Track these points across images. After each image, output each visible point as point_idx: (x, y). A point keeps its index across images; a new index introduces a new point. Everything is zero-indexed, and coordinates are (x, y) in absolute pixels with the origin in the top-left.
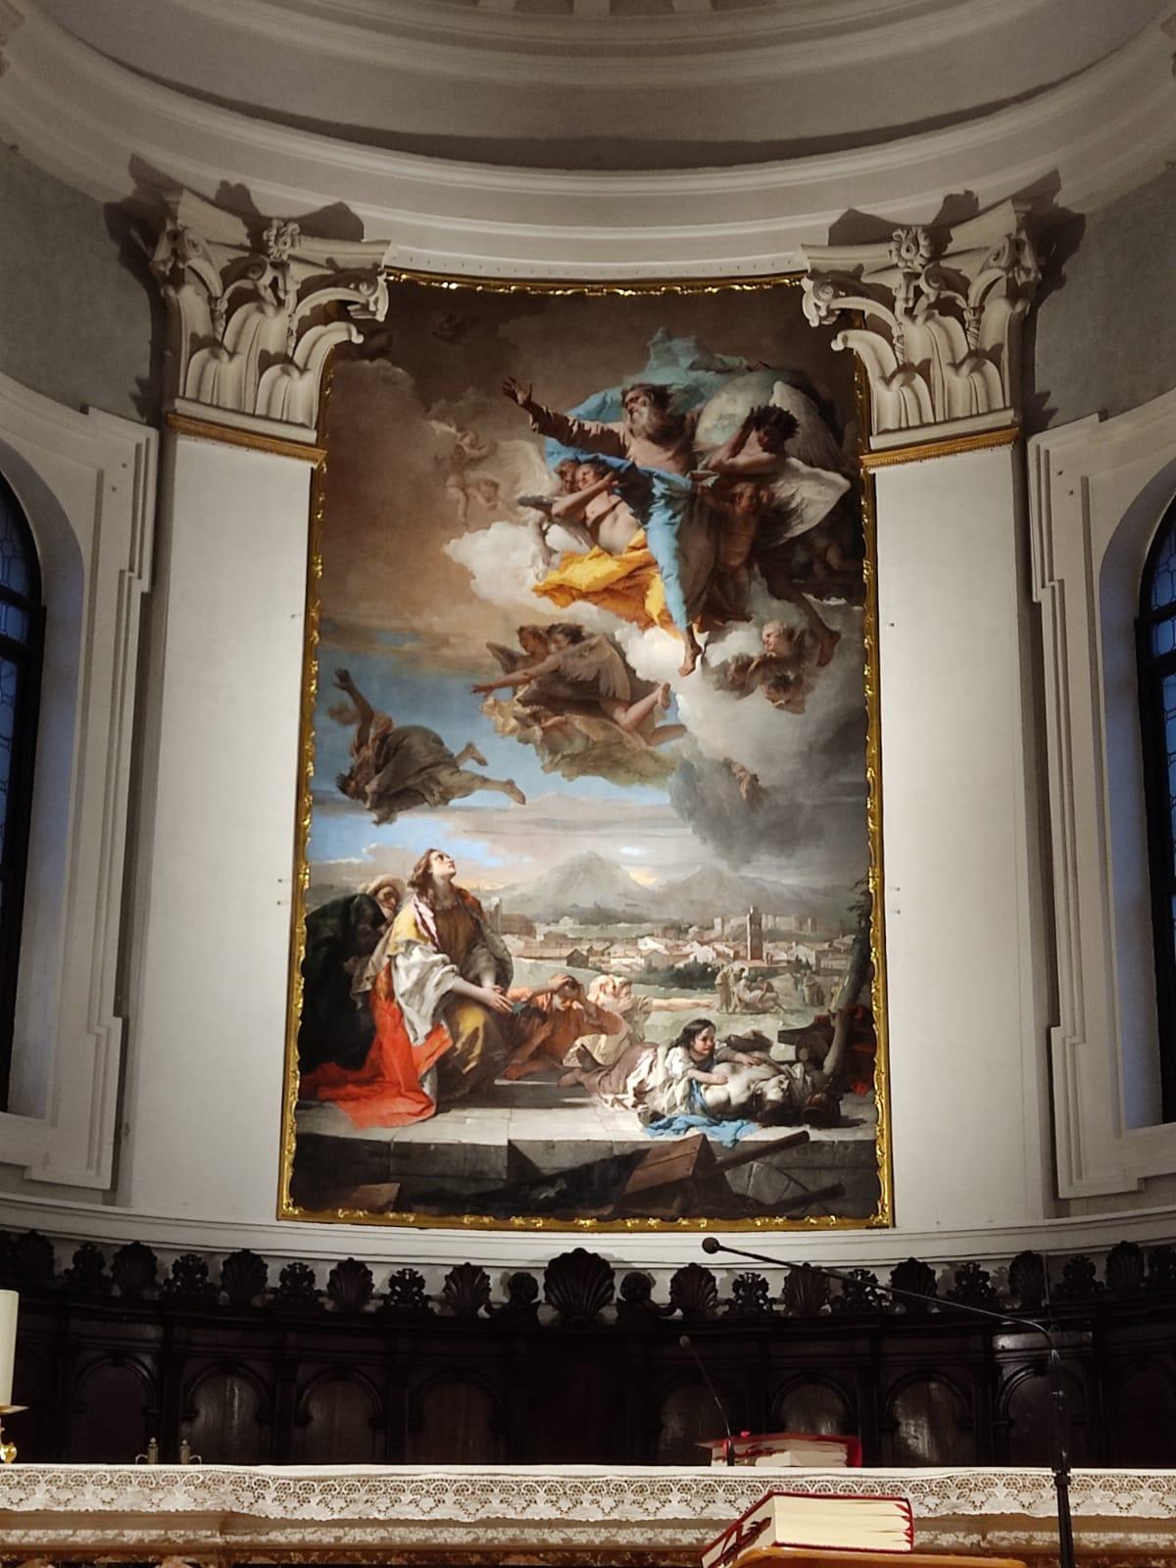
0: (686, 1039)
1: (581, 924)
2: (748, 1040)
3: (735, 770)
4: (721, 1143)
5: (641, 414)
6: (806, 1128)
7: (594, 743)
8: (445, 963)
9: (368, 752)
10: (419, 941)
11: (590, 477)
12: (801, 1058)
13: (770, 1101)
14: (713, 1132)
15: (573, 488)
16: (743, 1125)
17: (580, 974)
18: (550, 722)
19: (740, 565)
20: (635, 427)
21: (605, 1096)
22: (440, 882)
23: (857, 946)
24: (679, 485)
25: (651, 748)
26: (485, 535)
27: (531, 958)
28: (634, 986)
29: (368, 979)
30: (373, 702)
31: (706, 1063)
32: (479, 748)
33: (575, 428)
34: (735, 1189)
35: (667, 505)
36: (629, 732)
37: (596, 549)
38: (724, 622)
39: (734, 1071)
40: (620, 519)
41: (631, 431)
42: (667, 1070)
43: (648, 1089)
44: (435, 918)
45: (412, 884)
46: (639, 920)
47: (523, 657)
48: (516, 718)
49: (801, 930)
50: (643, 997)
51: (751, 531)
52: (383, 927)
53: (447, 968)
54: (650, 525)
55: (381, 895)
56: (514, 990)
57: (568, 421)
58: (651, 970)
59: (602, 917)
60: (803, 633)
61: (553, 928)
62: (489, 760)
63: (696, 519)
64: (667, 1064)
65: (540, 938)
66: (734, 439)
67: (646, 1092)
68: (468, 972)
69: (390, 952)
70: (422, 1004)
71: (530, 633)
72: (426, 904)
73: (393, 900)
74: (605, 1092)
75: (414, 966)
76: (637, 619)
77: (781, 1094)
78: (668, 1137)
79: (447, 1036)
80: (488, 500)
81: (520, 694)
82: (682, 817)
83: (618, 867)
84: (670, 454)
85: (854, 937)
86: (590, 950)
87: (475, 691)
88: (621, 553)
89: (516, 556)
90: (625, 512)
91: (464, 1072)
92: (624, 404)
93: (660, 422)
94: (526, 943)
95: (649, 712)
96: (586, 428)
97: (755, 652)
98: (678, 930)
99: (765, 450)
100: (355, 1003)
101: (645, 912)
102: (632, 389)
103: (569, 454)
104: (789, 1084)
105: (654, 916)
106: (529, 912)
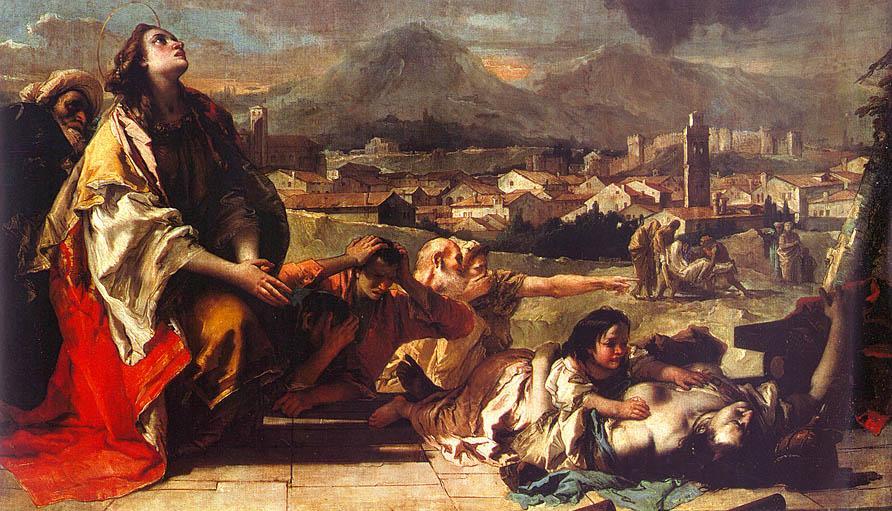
8: (173, 223)
14: (624, 499)
16: (675, 486)
21: (444, 441)
22: (161, 82)
27: (318, 210)
29: (44, 251)
31: (612, 383)
39: (661, 396)
42: (549, 396)
43: (517, 427)
44: (152, 146)
45: (113, 86)
46: (496, 142)
49: (775, 152)
53: (177, 231)
55: (61, 106)
58: (519, 225)
61: (354, 158)
65: (333, 175)
69: (80, 203)
72: (138, 121)
73: (81, 115)
74: (445, 434)
75: (121, 227)
77: (738, 434)
86: (417, 196)
94: (310, 184)
98: (562, 157)
101: (510, 128)
106: (315, 130)
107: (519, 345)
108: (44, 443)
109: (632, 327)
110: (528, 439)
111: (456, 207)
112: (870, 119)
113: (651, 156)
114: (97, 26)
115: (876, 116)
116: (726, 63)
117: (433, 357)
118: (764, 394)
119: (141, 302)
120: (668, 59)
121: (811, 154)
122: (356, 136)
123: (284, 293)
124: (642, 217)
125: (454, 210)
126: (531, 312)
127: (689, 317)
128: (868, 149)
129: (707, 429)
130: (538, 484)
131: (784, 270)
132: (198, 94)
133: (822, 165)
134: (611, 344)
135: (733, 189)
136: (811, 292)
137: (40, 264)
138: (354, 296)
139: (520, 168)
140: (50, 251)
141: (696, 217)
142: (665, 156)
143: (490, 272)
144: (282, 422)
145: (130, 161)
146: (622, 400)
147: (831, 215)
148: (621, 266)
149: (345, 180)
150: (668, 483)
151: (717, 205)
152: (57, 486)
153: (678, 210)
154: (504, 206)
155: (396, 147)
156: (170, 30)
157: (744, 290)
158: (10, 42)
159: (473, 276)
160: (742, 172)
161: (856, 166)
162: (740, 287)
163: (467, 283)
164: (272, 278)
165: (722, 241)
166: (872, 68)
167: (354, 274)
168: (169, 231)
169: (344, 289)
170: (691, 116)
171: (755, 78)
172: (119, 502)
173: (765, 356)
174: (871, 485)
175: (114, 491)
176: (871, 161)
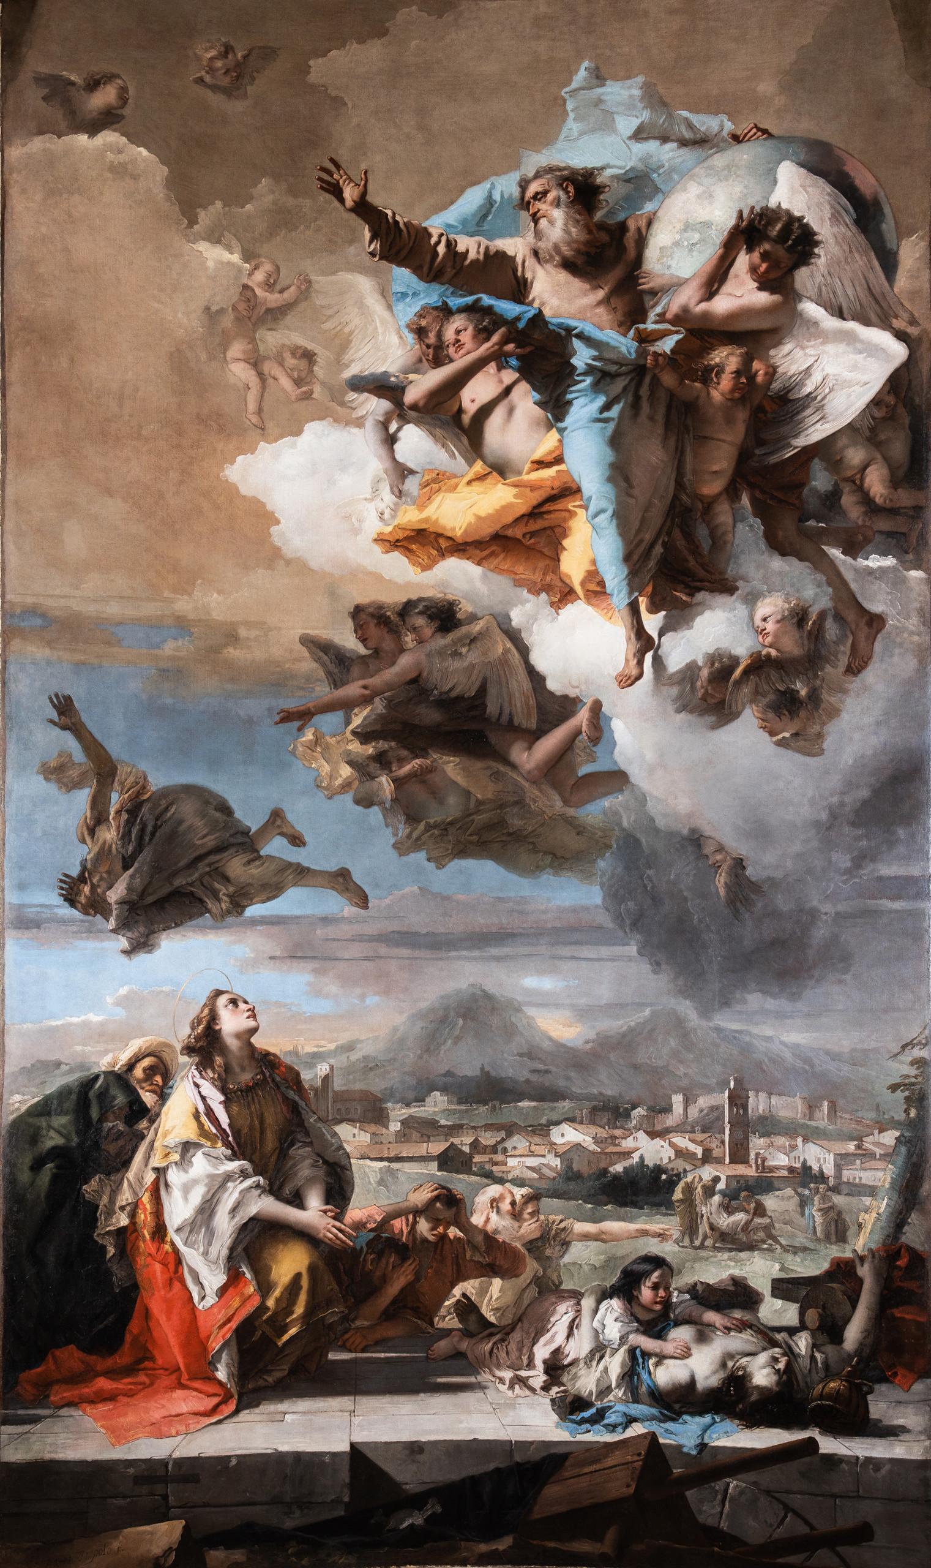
0: (626, 1287)
3: (708, 849)
4: (680, 1447)
5: (551, 222)
6: (814, 1433)
7: (479, 803)
8: (244, 1174)
9: (109, 835)
10: (203, 1141)
12: (809, 1324)
13: (758, 1387)
14: (666, 1430)
15: (438, 357)
16: (714, 1422)
17: (460, 1183)
18: (407, 769)
19: (720, 494)
20: (542, 245)
21: (499, 1373)
22: (233, 1043)
25: (571, 812)
27: (381, 1159)
28: (545, 1201)
29: (122, 1208)
31: (656, 1323)
33: (441, 249)
35: (596, 387)
37: (479, 467)
38: (692, 595)
39: (703, 1336)
40: (518, 413)
41: (536, 253)
42: (596, 1333)
43: (566, 1362)
44: (227, 1103)
45: (189, 1050)
48: (350, 763)
49: (811, 1118)
50: (560, 1217)
52: (144, 1124)
53: (249, 1182)
54: (569, 421)
55: (138, 1072)
56: (355, 1212)
57: (430, 236)
58: (570, 1175)
59: (489, 1091)
60: (822, 615)
61: (414, 1110)
64: (596, 1324)
65: (395, 1127)
66: (709, 268)
68: (281, 1187)
69: (156, 1161)
71: (372, 615)
73: (158, 1079)
74: (499, 1366)
75: (195, 1182)
76: (547, 588)
77: (775, 1378)
78: (597, 1436)
80: (298, 382)
81: (357, 721)
82: (622, 927)
84: (601, 294)
85: (898, 1134)
86: (475, 1145)
88: (520, 473)
89: (345, 481)
90: (525, 399)
91: (280, 1344)
94: (373, 1134)
95: (568, 746)
96: (461, 248)
97: (743, 647)
98: (611, 1113)
99: (760, 288)
101: (562, 1083)
102: (537, 176)
104: (788, 1364)
106: (377, 1085)
108: (120, 1386)
111: (511, 1156)
113: (694, 1112)
115: (907, 1093)
119: (214, 1251)
120: (711, 1024)
123: (349, 1236)
124: (685, 1171)
125: (509, 1159)
126: (580, 1253)
127: (729, 1267)
129: (745, 1371)
130: (586, 1414)
131: (819, 1229)
134: (655, 1287)
138: (415, 1239)
139: (571, 1120)
140: (128, 1208)
142: (707, 1115)
146: (665, 1340)
147: (864, 1182)
148: (665, 1215)
149: (407, 1131)
150: (708, 1419)
151: (756, 1163)
155: (455, 1099)
157: (781, 1245)
159: (526, 1220)
161: (889, 1138)
162: (778, 1242)
163: (520, 1227)
164: (338, 1224)
166: (904, 1047)
169: (405, 1232)
173: (801, 1307)
174: (901, 1438)
176: (902, 1135)
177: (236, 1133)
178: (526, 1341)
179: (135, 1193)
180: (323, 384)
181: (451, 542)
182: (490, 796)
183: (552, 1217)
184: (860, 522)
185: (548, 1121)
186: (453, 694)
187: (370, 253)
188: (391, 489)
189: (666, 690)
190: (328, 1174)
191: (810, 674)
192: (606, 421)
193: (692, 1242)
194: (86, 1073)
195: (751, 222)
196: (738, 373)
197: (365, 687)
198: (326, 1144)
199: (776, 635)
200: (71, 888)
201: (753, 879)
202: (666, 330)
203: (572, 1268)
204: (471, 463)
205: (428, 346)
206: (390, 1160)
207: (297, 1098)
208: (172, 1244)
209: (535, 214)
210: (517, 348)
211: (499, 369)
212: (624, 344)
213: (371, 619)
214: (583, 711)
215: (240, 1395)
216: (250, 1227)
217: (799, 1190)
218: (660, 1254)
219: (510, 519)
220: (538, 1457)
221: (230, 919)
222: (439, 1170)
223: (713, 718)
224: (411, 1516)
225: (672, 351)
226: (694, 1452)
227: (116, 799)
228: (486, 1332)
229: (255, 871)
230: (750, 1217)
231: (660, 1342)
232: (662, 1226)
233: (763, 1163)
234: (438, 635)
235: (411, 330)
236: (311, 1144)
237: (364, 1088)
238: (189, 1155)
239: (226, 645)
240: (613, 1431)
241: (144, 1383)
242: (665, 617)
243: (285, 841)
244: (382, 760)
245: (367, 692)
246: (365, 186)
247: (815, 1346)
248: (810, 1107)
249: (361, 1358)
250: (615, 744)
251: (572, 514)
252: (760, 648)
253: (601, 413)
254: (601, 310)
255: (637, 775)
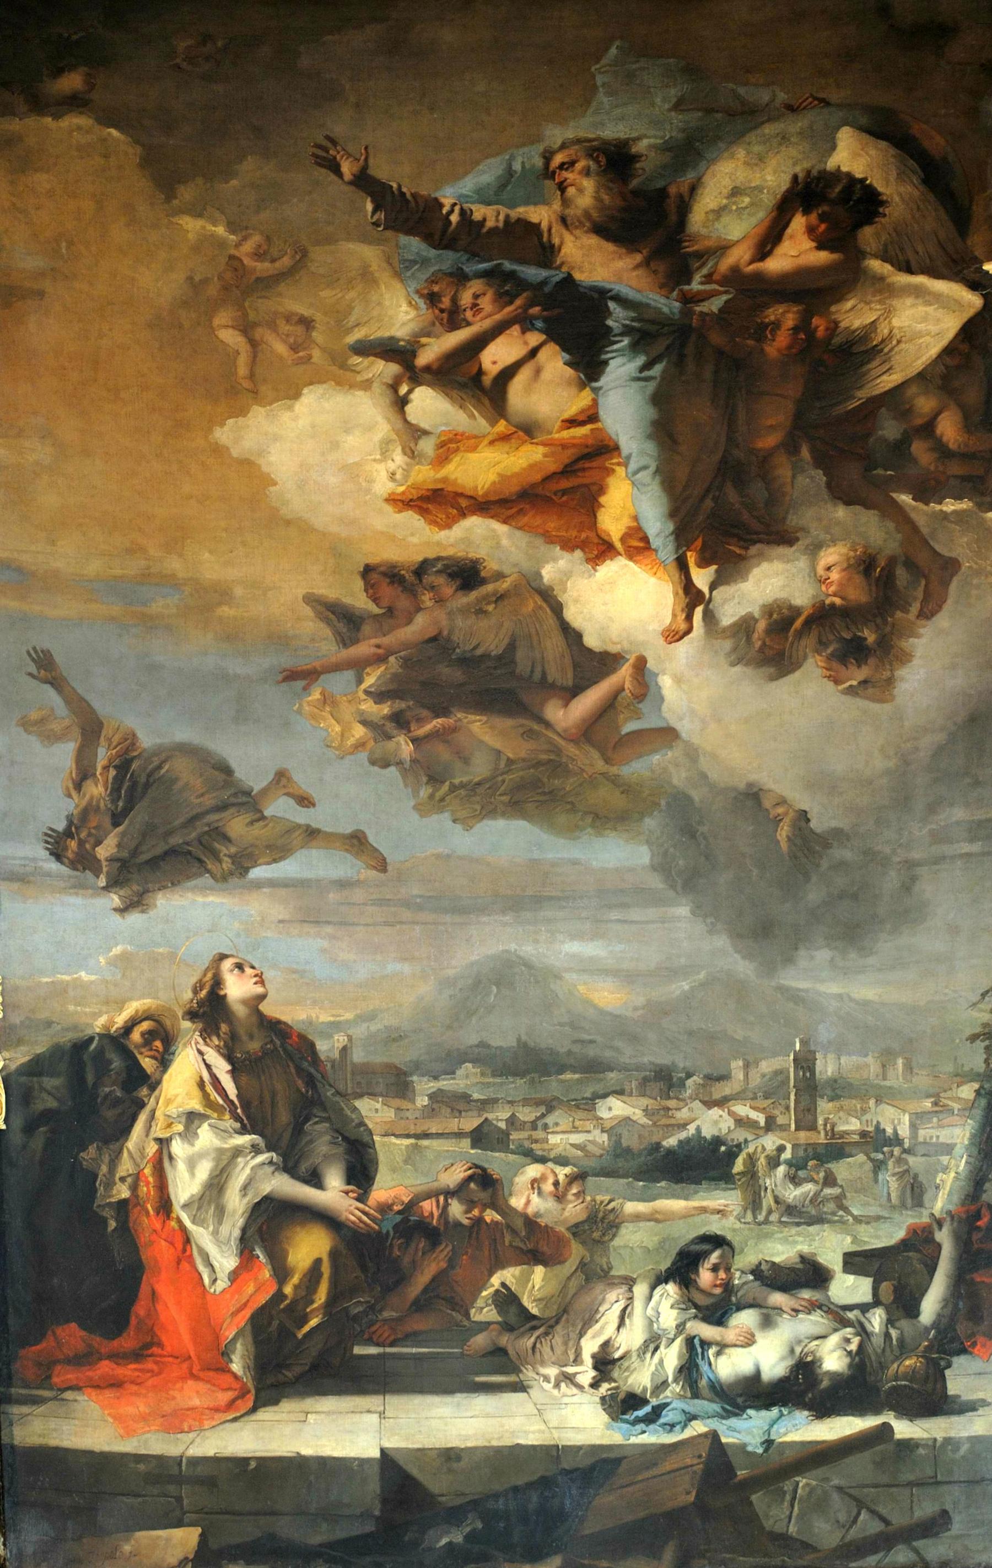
0: (682, 1268)
1: (494, 1075)
2: (792, 1269)
3: (767, 804)
4: (744, 1446)
5: (581, 190)
6: (888, 1417)
7: (510, 762)
8: (256, 1150)
9: (96, 790)
10: (209, 1112)
11: (486, 303)
12: (883, 1299)
13: (828, 1373)
14: (729, 1428)
15: (453, 320)
16: (782, 1415)
17: (496, 1162)
18: (428, 728)
19: (777, 447)
20: (570, 212)
21: (544, 1371)
22: (240, 1011)
23: (983, 1102)
24: (659, 311)
25: (614, 770)
26: (290, 408)
27: (408, 1136)
28: (591, 1180)
29: (123, 1179)
30: (102, 707)
31: (717, 1312)
32: (298, 777)
33: (454, 218)
34: (768, 1524)
35: (635, 348)
36: (574, 741)
37: (502, 426)
38: (747, 549)
39: (767, 1322)
40: (546, 375)
41: (563, 220)
42: (651, 1323)
43: (617, 1355)
44: (234, 1073)
45: (192, 1015)
46: (593, 1067)
47: (376, 617)
48: (364, 723)
49: (884, 1079)
50: (607, 1198)
51: (794, 389)
52: (144, 1091)
53: (261, 1158)
54: (603, 381)
55: (136, 1036)
56: (382, 1191)
57: (441, 206)
58: (619, 1151)
59: (530, 1064)
60: (892, 561)
61: (445, 1084)
62: (314, 793)
63: (691, 366)
64: (650, 1312)
65: (422, 1101)
66: (761, 230)
67: (614, 1361)
68: (297, 1163)
69: (159, 1131)
70: (220, 1222)
71: (385, 574)
72: (218, 1048)
73: (158, 1044)
74: (543, 1363)
75: (202, 1155)
76: (583, 545)
77: (847, 1360)
78: (652, 1437)
79: (267, 1273)
80: (294, 348)
81: (370, 680)
82: (673, 887)
83: (558, 977)
84: (638, 258)
85: (976, 1086)
86: (512, 1121)
87: (286, 679)
88: (551, 433)
89: (352, 441)
90: (554, 362)
91: (300, 1335)
92: (548, 174)
93: (619, 202)
94: (398, 1109)
95: (609, 707)
96: (477, 216)
97: (802, 595)
98: (665, 1081)
99: (820, 247)
100: (105, 1222)
101: (608, 1054)
102: (563, 147)
103: (449, 259)
104: (861, 1346)
105: (624, 1059)
106: (401, 1056)
107: (619, 1270)
108: (129, 1373)
109: (737, 1251)
110: (628, 1367)
112: (980, 1045)
113: (755, 1080)
114: (172, 956)
115: (987, 1043)
116: (833, 988)
117: (530, 1285)
118: (873, 1320)
119: (225, 1229)
120: (773, 984)
121: (922, 1080)
122: (451, 1061)
123: (373, 1219)
124: (746, 1141)
125: (550, 1136)
128: (979, 1075)
132: (279, 1022)
133: (931, 1091)
134: (715, 1269)
135: (841, 1114)
136: (921, 1216)
137: (119, 1192)
138: (447, 1222)
139: (619, 1093)
140: (129, 1180)
141: (802, 1142)
142: (770, 1080)
143: (588, 1198)
144: (373, 1350)
145: (209, 1088)
147: (941, 1140)
148: (725, 1190)
149: (435, 1106)
150: (775, 1411)
152: (144, 1418)
153: (784, 1134)
154: (603, 1131)
155: (489, 1072)
156: (249, 958)
157: (852, 1215)
158: (83, 974)
159: (571, 1202)
160: (850, 1097)
161: (967, 1092)
165: (830, 1165)
167: (446, 1200)
168: (253, 1158)
169: (436, 1214)
170: (797, 1040)
171: (865, 1004)
172: (207, 1433)
175: (201, 1421)
176: (982, 1087)
177: (246, 1105)
178: (572, 1335)
179: (136, 1164)
180: (323, 350)
181: (472, 501)
182: (523, 754)
183: (599, 1198)
184: (932, 468)
185: (593, 1093)
186: (479, 652)
187: (373, 224)
188: (403, 449)
189: (718, 643)
190: (348, 1152)
191: (879, 620)
192: (646, 379)
193: (755, 1217)
194: (81, 1035)
195: (807, 185)
196: (796, 329)
197: (378, 646)
198: (346, 1120)
199: (840, 584)
200: (57, 843)
201: (818, 831)
202: (715, 290)
203: (622, 1252)
204: (493, 423)
205: (442, 311)
206: (417, 1137)
207: (312, 1070)
208: (179, 1221)
209: (562, 183)
210: (544, 310)
211: (523, 332)
212: (666, 304)
213: (383, 577)
214: (624, 668)
215: (258, 1390)
216: (263, 1207)
217: (873, 1155)
218: (719, 1233)
219: (538, 477)
220: (588, 1462)
221: (235, 881)
222: (472, 1148)
223: (772, 670)
224: (448, 1532)
225: (720, 310)
226: (760, 1451)
227: (103, 755)
228: (528, 1326)
229: (257, 831)
230: (819, 1187)
231: (720, 1329)
232: (722, 1201)
233: (833, 1130)
234: (460, 593)
235: (422, 296)
236: (328, 1119)
237: (385, 1060)
238: (194, 1126)
239: (220, 604)
240: (671, 1431)
241: (152, 1371)
242: (717, 571)
243: (291, 802)
244: (400, 720)
245: (380, 651)
246: (366, 159)
247: (890, 1322)
248: (884, 1066)
249: (390, 1354)
250: (662, 699)
251: (610, 472)
252: (823, 598)
253: (641, 371)
254: (640, 272)
255: (685, 728)
